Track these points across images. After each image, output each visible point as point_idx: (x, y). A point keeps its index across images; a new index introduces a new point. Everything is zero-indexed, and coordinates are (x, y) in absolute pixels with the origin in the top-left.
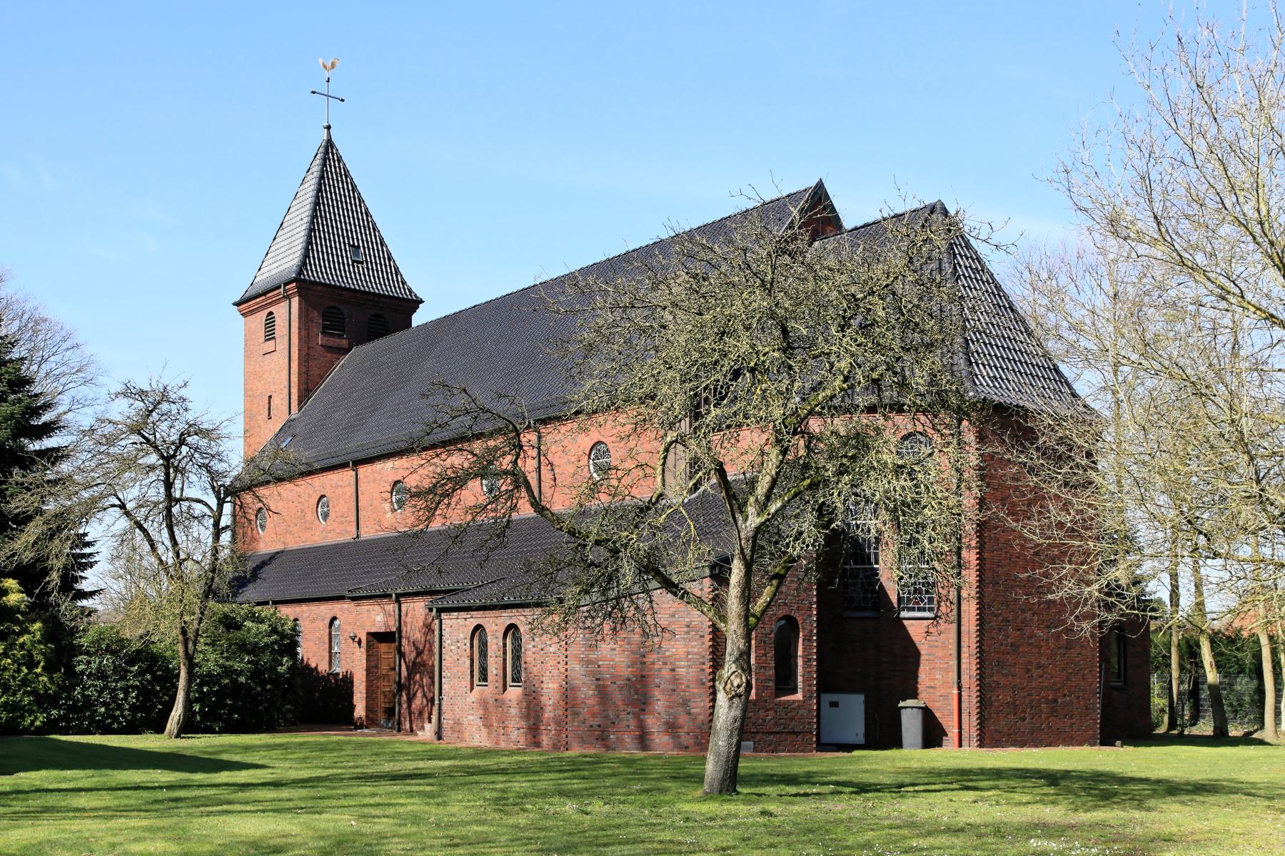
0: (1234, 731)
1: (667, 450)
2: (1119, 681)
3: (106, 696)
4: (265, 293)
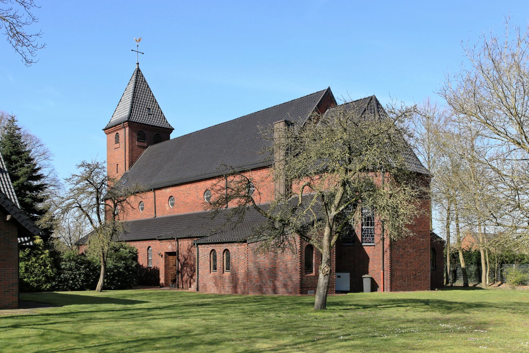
0: (471, 285)
1: (303, 188)
2: (433, 265)
3: (73, 276)
4: (115, 126)
